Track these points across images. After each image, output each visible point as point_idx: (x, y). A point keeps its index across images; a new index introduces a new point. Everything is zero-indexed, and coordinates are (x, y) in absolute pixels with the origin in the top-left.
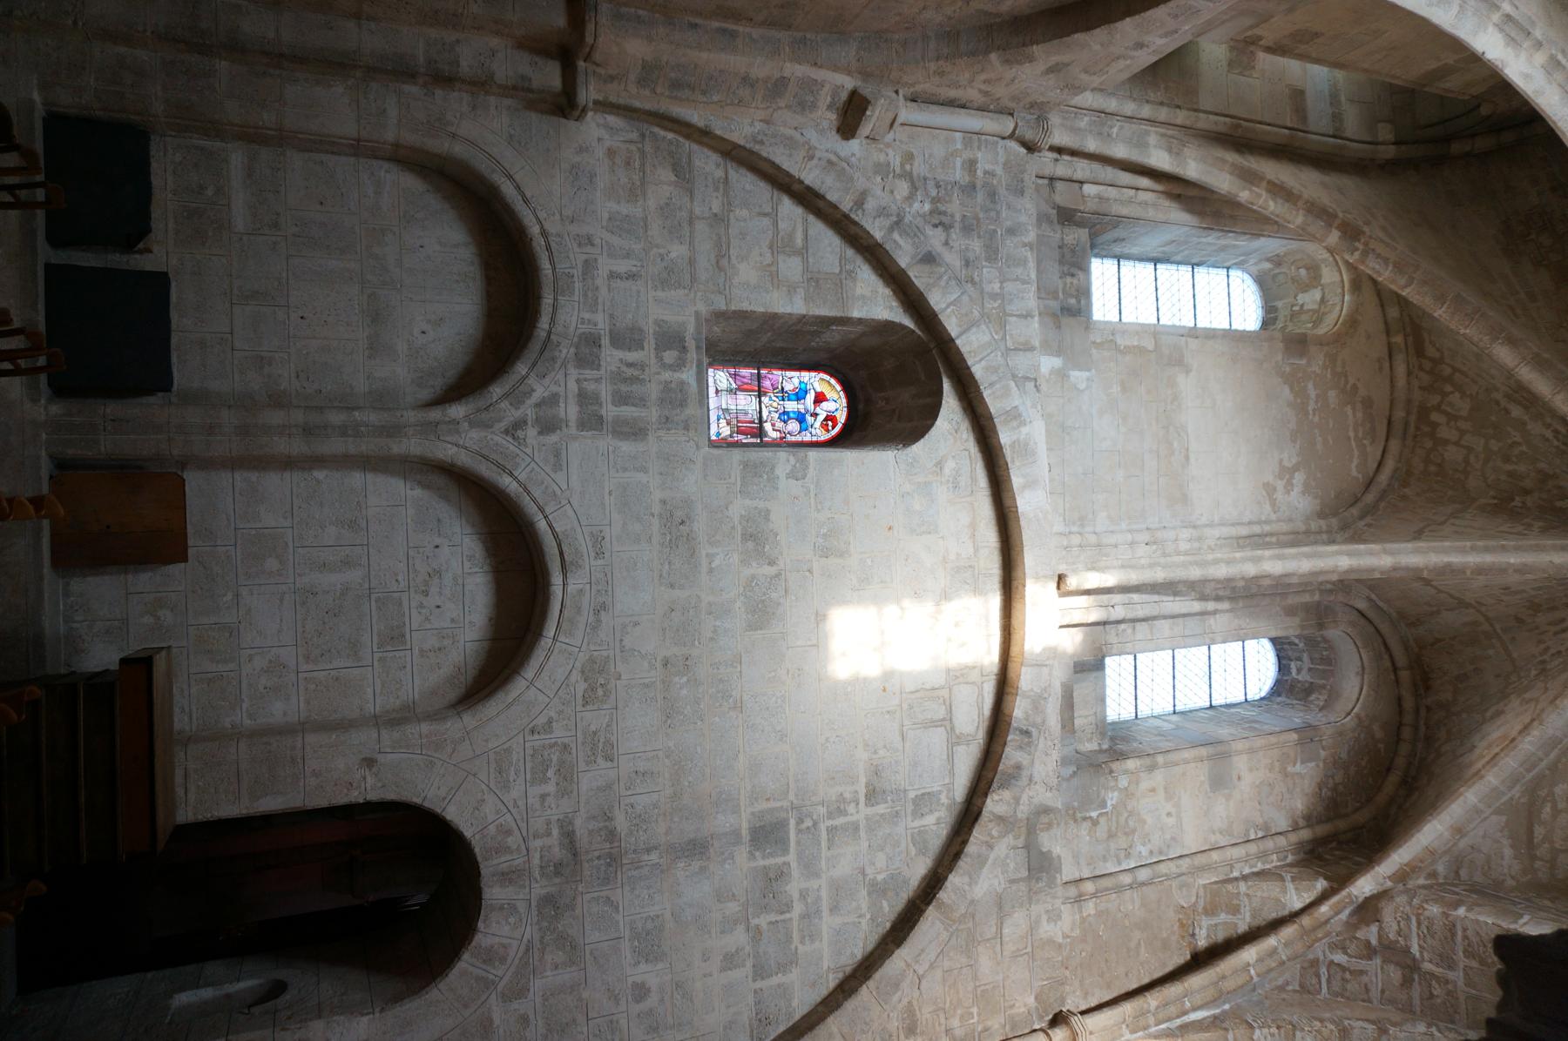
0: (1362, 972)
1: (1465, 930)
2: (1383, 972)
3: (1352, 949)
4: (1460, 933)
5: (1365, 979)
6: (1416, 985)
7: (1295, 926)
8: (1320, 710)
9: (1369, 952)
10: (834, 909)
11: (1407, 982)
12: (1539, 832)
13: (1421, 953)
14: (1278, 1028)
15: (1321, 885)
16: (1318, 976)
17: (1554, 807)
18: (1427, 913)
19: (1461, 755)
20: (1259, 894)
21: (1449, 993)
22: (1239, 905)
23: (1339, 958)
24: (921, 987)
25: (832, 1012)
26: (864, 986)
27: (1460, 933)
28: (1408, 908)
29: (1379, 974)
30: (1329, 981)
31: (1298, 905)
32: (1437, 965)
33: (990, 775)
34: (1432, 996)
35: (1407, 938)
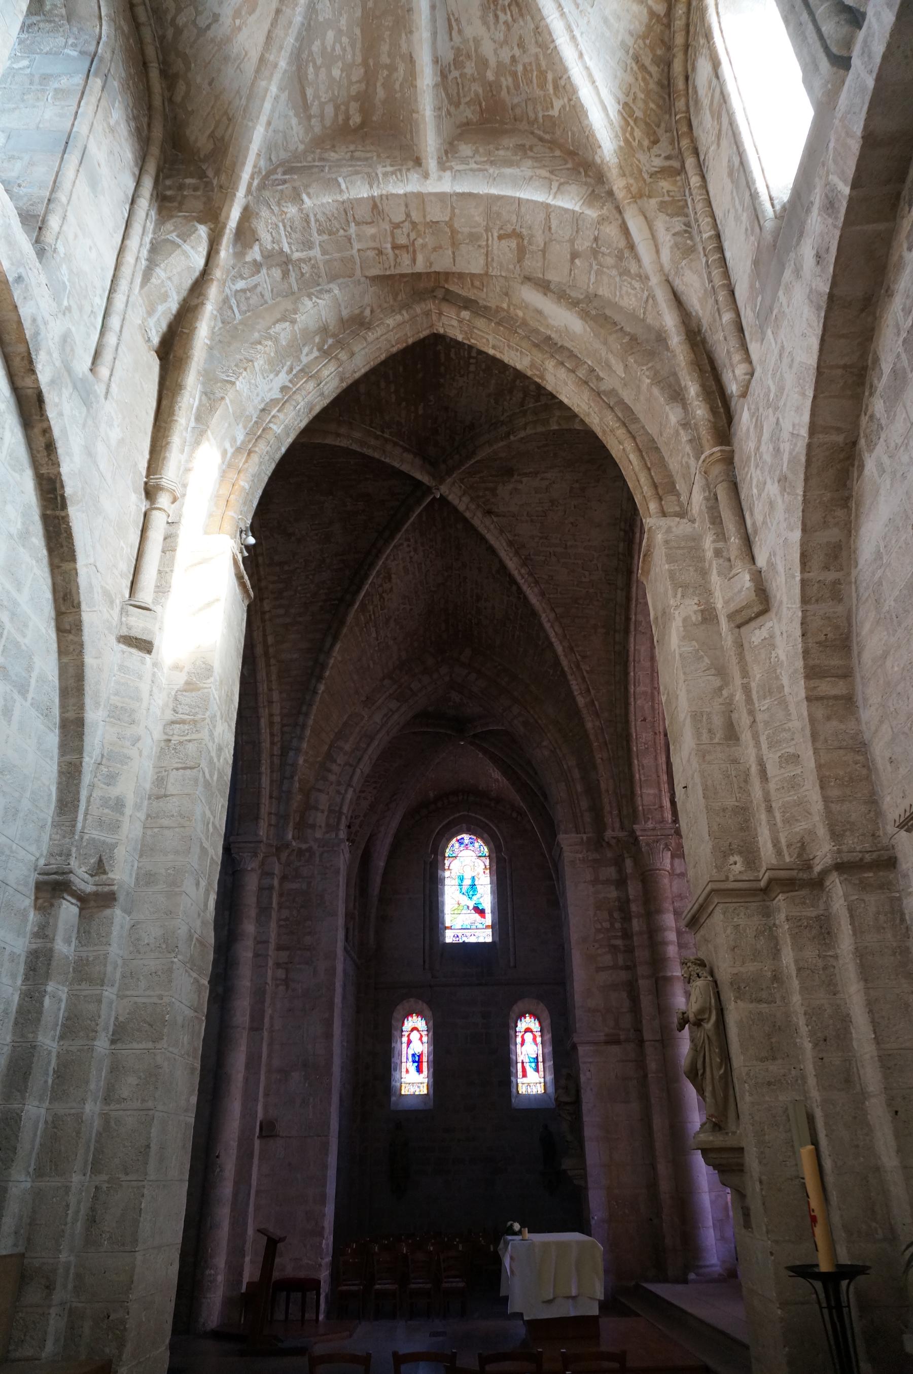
0: (256, 286)
1: (315, 215)
2: (269, 277)
3: (246, 272)
4: (312, 219)
5: (259, 289)
6: (292, 274)
7: (215, 283)
8: (69, 21)
9: (257, 267)
10: (19, 587)
11: (285, 274)
12: (309, 92)
13: (290, 248)
14: (245, 369)
15: (203, 231)
16: (231, 308)
17: (315, 64)
18: (288, 216)
19: (209, 27)
20: (175, 271)
21: (313, 267)
22: (166, 292)
23: (241, 285)
24: (100, 570)
25: (81, 653)
26: (83, 613)
27: (312, 219)
28: (274, 218)
29: (267, 279)
30: (238, 306)
31: (199, 262)
32: (302, 251)
33: (21, 349)
34: (302, 274)
35: (279, 242)
